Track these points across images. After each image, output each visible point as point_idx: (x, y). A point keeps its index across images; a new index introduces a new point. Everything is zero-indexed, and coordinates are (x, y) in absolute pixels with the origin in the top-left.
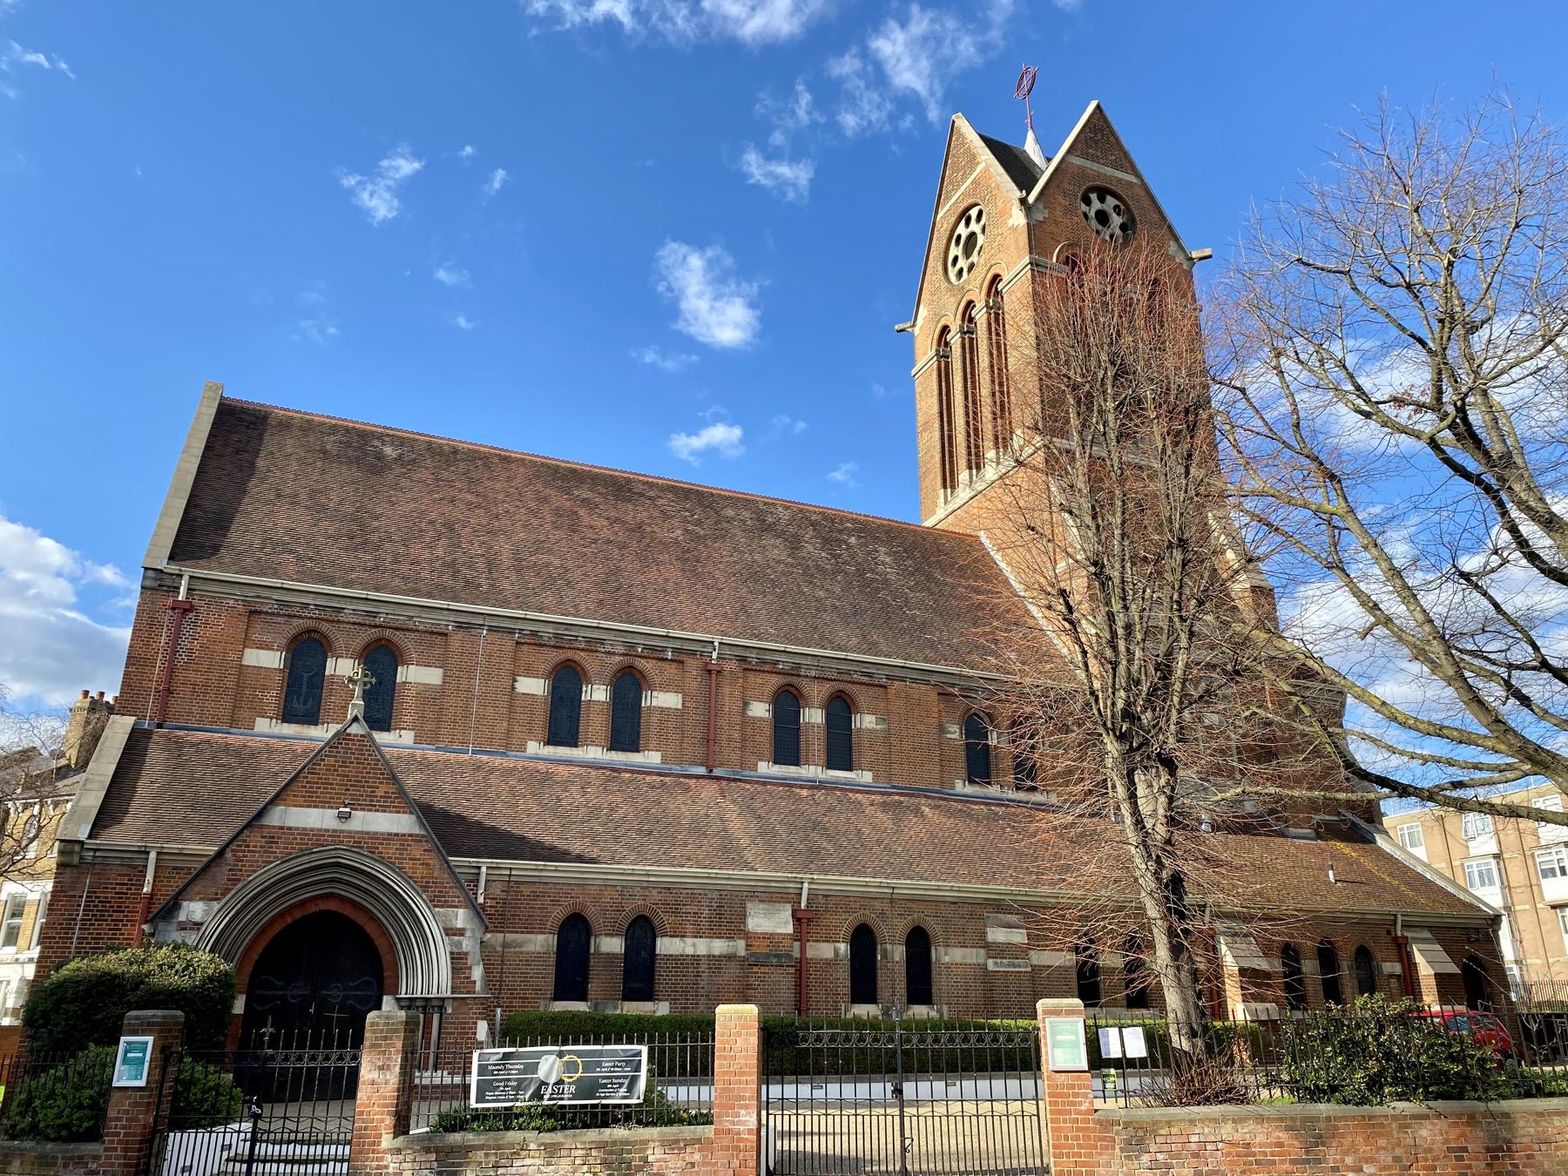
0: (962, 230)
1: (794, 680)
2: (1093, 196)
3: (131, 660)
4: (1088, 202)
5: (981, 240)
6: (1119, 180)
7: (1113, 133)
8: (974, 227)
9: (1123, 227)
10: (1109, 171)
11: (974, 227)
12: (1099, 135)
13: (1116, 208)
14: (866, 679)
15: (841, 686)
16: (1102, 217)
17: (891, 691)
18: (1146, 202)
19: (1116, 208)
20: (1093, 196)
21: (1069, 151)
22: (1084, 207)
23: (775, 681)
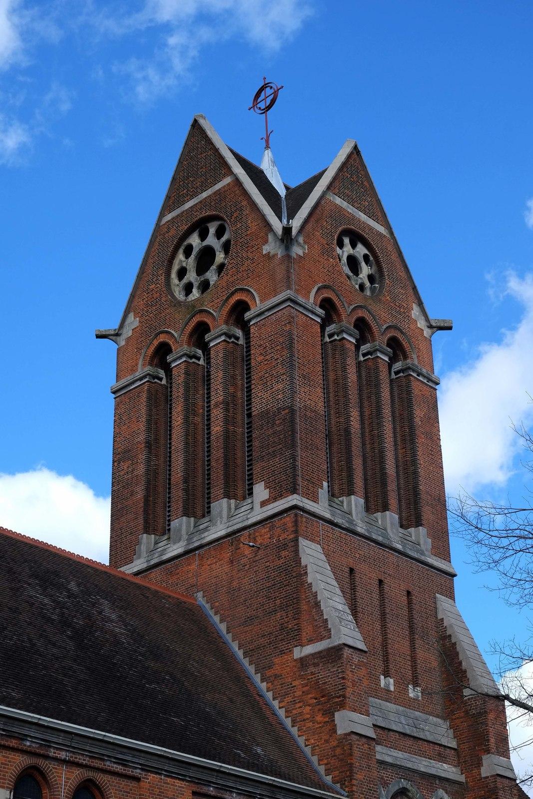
0: (194, 240)
1: (41, 763)
2: (347, 241)
3: (410, 401)
4: (341, 245)
5: (220, 257)
6: (371, 229)
7: (367, 176)
8: (211, 240)
9: (371, 278)
10: (363, 217)
11: (211, 240)
12: (354, 174)
13: (366, 257)
14: (118, 768)
15: (90, 774)
16: (353, 262)
17: (145, 784)
18: (394, 257)
19: (366, 257)
20: (347, 241)
21: (329, 187)
22: (339, 251)
23: (19, 761)
